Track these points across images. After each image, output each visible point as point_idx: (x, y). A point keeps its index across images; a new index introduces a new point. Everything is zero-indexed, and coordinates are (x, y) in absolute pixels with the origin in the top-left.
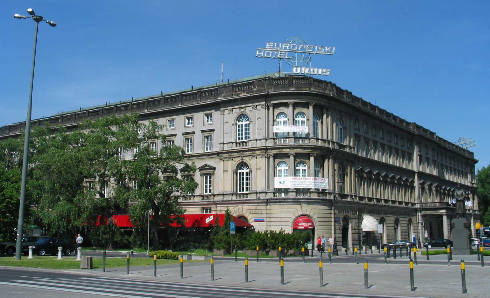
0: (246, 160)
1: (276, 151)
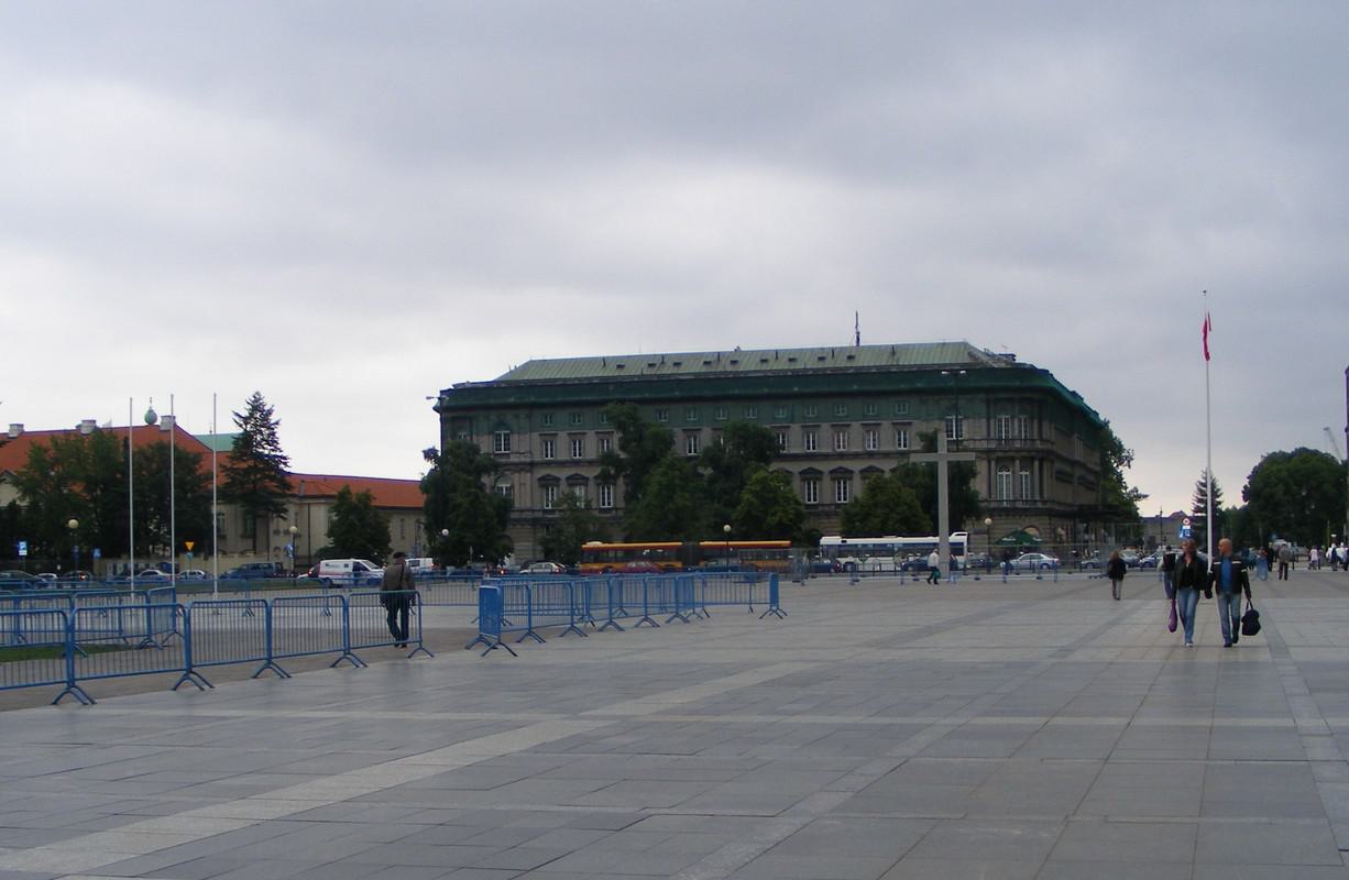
1: (1000, 454)
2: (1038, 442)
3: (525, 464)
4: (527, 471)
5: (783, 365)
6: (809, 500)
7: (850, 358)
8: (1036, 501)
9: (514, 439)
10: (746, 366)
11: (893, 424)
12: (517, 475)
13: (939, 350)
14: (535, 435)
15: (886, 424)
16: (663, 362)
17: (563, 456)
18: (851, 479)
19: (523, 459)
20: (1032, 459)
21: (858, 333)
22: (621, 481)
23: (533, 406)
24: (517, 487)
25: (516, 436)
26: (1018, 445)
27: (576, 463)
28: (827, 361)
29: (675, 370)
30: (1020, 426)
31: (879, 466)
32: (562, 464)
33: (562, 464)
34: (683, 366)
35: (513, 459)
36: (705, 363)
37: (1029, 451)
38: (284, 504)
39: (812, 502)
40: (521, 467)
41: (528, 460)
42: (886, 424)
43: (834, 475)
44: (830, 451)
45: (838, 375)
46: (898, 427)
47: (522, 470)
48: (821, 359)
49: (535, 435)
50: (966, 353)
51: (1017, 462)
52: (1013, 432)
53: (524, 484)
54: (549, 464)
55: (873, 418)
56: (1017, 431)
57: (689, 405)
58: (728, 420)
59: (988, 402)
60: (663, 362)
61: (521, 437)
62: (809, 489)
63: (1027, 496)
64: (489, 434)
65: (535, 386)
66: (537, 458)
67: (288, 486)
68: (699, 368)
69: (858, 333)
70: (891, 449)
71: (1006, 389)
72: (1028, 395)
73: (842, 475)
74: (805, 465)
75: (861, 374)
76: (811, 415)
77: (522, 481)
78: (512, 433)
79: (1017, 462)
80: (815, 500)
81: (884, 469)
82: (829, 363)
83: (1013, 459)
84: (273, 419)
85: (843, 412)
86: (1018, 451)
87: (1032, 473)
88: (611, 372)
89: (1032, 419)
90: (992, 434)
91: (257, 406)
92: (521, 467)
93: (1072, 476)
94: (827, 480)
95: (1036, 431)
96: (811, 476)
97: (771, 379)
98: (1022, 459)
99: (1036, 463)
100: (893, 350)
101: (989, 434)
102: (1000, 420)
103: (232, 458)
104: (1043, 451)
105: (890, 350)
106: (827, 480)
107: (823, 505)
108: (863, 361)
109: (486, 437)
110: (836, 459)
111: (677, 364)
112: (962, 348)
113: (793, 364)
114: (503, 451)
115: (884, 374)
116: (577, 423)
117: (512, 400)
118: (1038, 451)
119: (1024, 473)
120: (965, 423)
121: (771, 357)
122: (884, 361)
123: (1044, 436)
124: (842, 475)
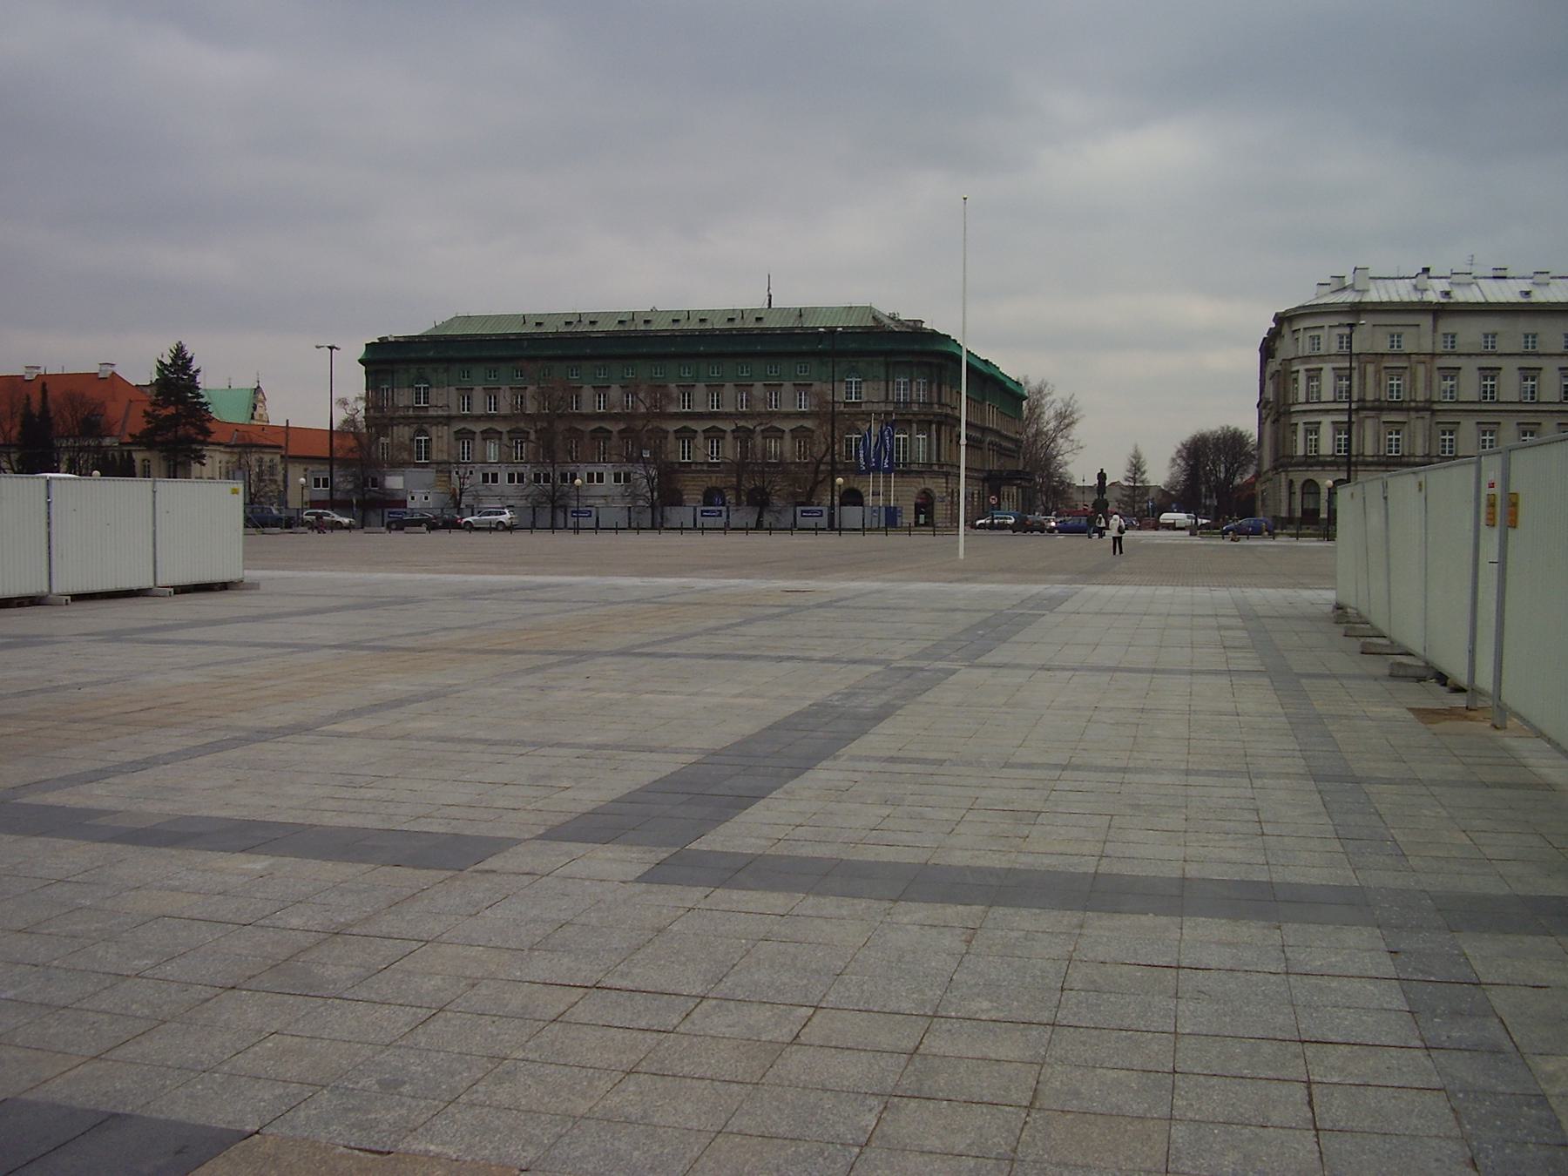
0: (426, 426)
2: (936, 406)
3: (442, 417)
4: (445, 425)
5: (694, 325)
6: (684, 458)
7: (759, 319)
8: (932, 464)
9: (433, 392)
10: (659, 325)
11: (794, 385)
12: (434, 428)
13: (844, 314)
14: (452, 389)
15: (788, 385)
16: (580, 321)
17: (478, 409)
18: (723, 438)
19: (440, 413)
20: (930, 423)
21: (770, 296)
22: (364, 430)
23: (450, 361)
24: (434, 439)
25: (435, 390)
26: (915, 408)
27: (491, 418)
28: (736, 321)
29: (590, 329)
30: (918, 390)
31: (609, 428)
32: (479, 418)
33: (479, 418)
34: (598, 325)
35: (432, 412)
36: (620, 322)
37: (925, 414)
38: (201, 450)
39: (686, 460)
40: (440, 420)
41: (445, 413)
42: (788, 385)
43: (707, 434)
44: (733, 410)
45: (745, 335)
46: (801, 388)
47: (440, 423)
48: (731, 320)
49: (452, 389)
50: (871, 316)
51: (915, 426)
52: (911, 396)
53: (442, 437)
54: (464, 418)
55: (773, 378)
56: (914, 395)
57: (599, 363)
58: (636, 378)
59: (887, 365)
60: (580, 321)
61: (440, 391)
62: (684, 447)
63: (923, 459)
64: (409, 387)
65: (454, 341)
66: (454, 412)
67: (208, 433)
68: (612, 326)
69: (770, 296)
70: (791, 409)
71: (908, 353)
72: (925, 359)
73: (714, 435)
74: (708, 425)
75: (812, 335)
76: (687, 375)
77: (440, 434)
78: (431, 386)
79: (915, 426)
80: (689, 458)
81: (669, 429)
82: (738, 324)
83: (910, 422)
84: (194, 366)
85: (747, 372)
86: (914, 414)
87: (929, 436)
88: (530, 329)
89: (930, 383)
90: (891, 398)
91: (180, 355)
92: (440, 420)
93: (982, 442)
94: (700, 440)
95: (935, 395)
96: (686, 435)
97: (679, 339)
98: (919, 422)
99: (934, 426)
100: (801, 313)
101: (887, 398)
102: (899, 384)
103: (153, 404)
104: (940, 414)
105: (797, 313)
106: (700, 440)
107: (696, 463)
108: (770, 323)
109: (406, 389)
110: (710, 419)
111: (593, 323)
112: (868, 311)
113: (676, 324)
114: (422, 405)
115: (788, 335)
116: (493, 378)
117: (431, 354)
118: (935, 415)
119: (920, 436)
120: (864, 385)
121: (683, 317)
122: (791, 323)
123: (943, 401)
124: (714, 435)
